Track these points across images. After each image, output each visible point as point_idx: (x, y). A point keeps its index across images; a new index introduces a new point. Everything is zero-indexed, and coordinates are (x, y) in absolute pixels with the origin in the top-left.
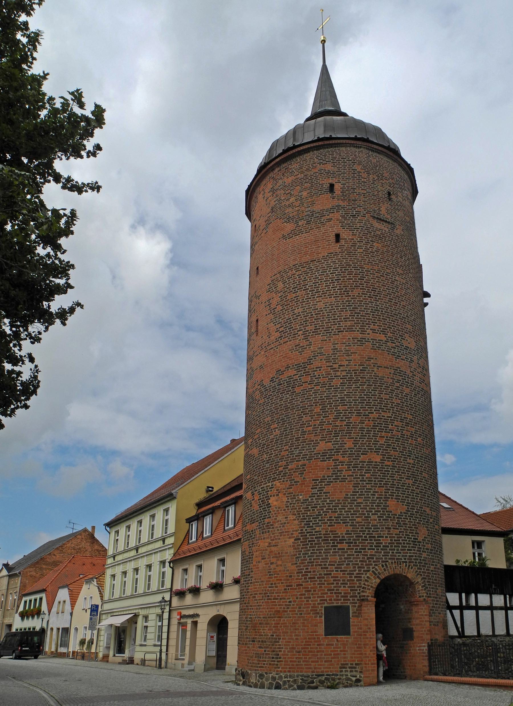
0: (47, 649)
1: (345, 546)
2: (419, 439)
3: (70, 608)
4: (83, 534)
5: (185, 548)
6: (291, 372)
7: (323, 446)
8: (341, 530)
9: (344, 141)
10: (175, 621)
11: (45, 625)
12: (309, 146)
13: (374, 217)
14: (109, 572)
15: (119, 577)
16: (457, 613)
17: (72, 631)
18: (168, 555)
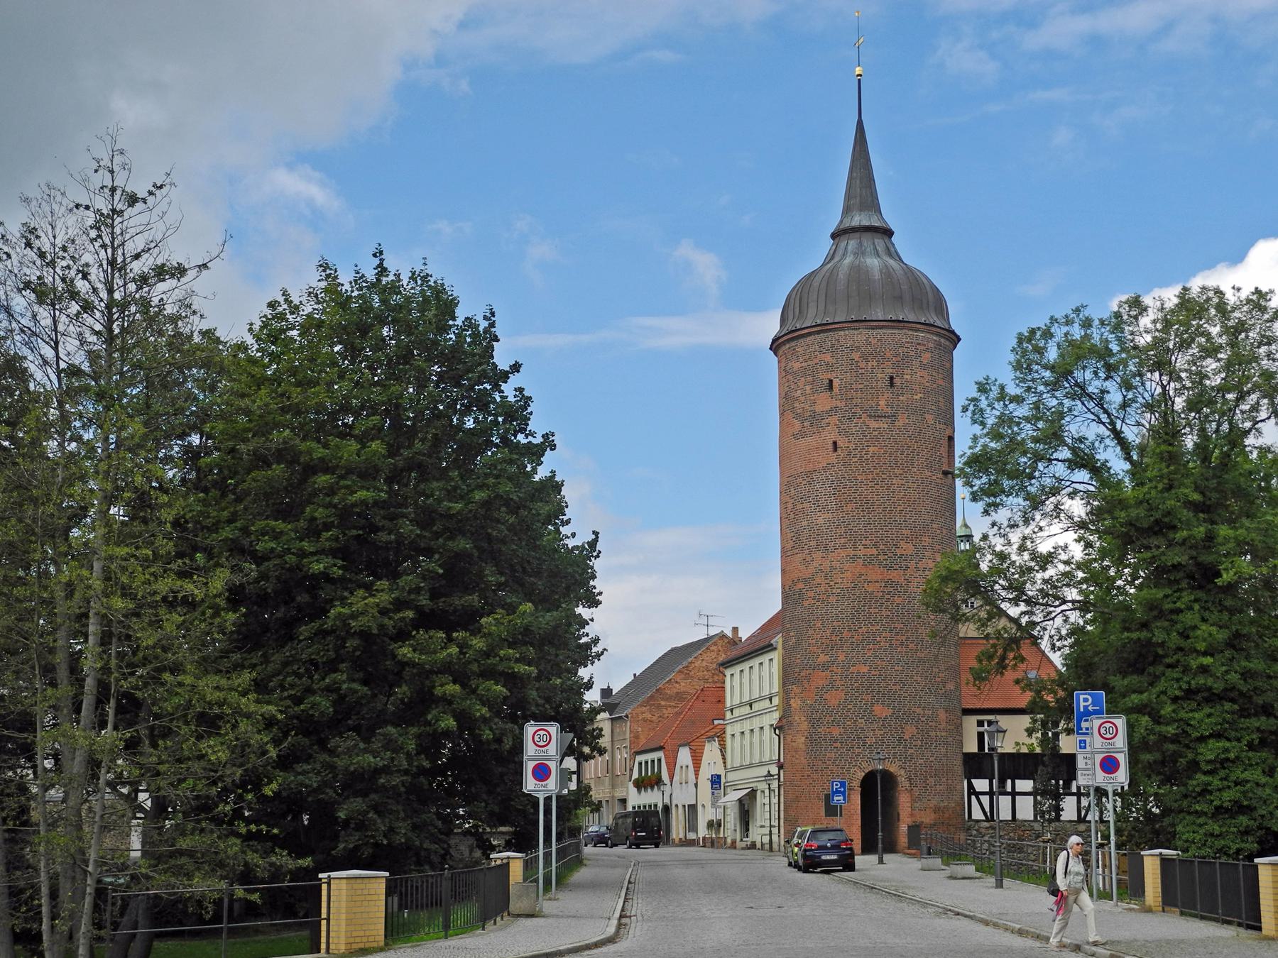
0: (674, 835)
1: (838, 745)
4: (720, 643)
7: (823, 658)
8: (836, 732)
11: (667, 801)
13: (870, 416)
14: (729, 730)
15: (738, 736)
17: (700, 808)
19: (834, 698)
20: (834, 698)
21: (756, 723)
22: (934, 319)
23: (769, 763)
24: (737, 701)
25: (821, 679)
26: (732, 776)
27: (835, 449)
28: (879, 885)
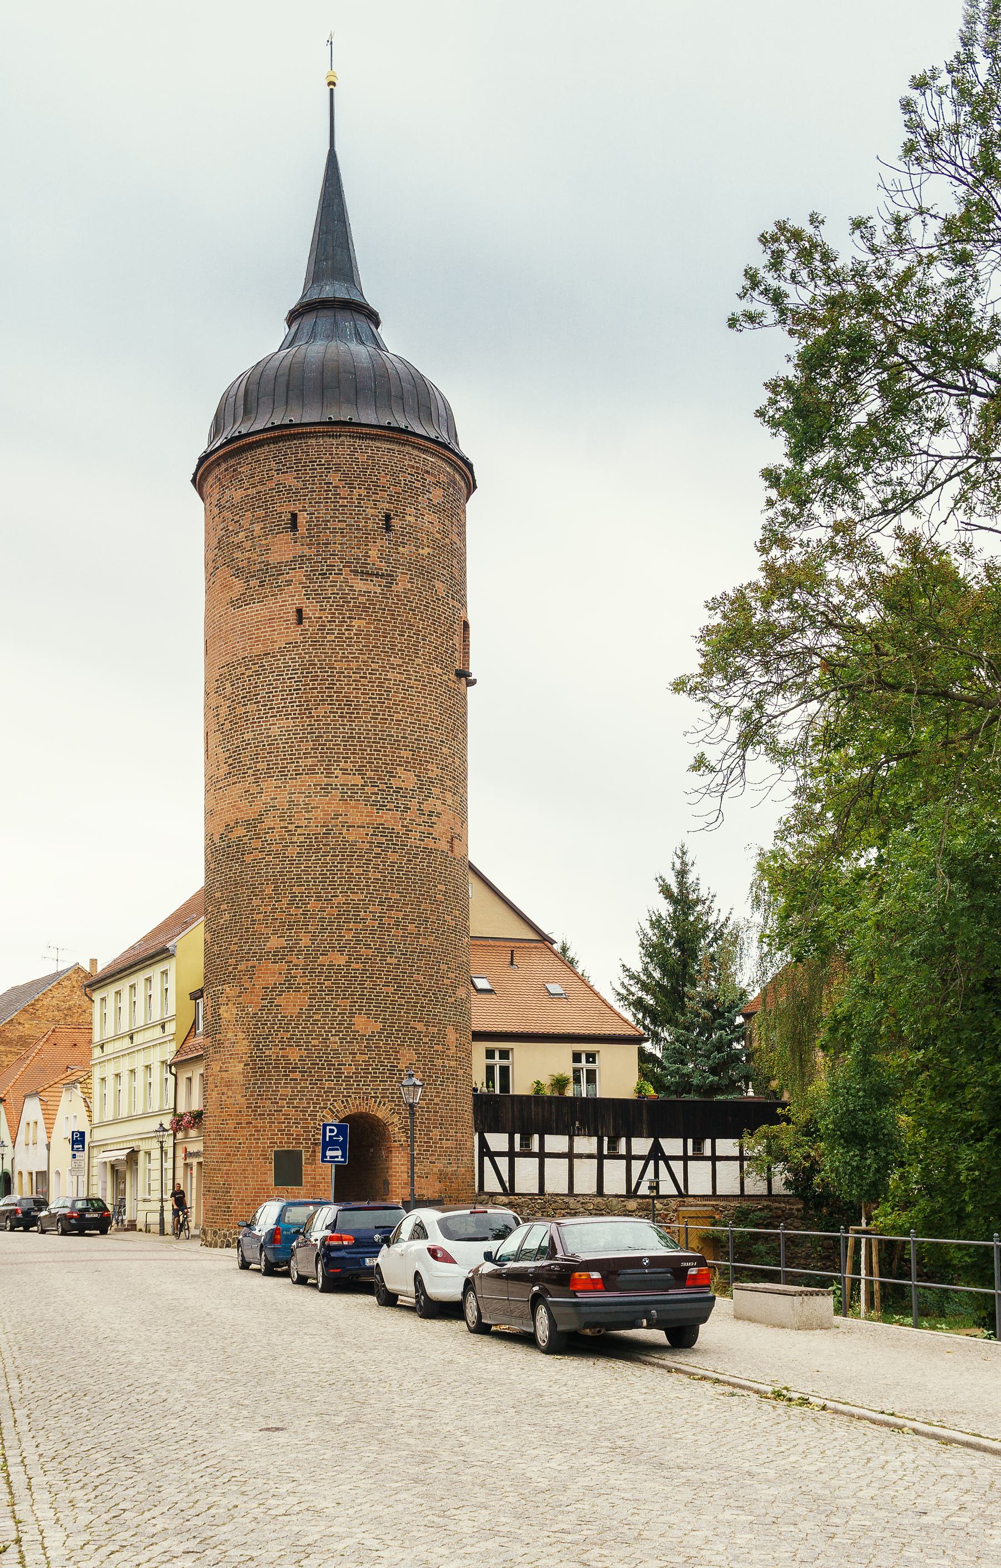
1: (298, 1075)
2: (410, 927)
3: (45, 1136)
5: (193, 1042)
6: (240, 831)
7: (275, 942)
8: (294, 1055)
9: (312, 429)
10: (180, 1162)
12: (261, 436)
14: (97, 1073)
15: (111, 1080)
16: (677, 1166)
17: (53, 1177)
18: (169, 1052)
19: (292, 1004)
20: (292, 1004)
21: (139, 1061)
22: (444, 438)
23: (161, 1113)
24: (110, 1032)
25: (271, 974)
26: (99, 1134)
27: (300, 621)
28: (799, 1388)
